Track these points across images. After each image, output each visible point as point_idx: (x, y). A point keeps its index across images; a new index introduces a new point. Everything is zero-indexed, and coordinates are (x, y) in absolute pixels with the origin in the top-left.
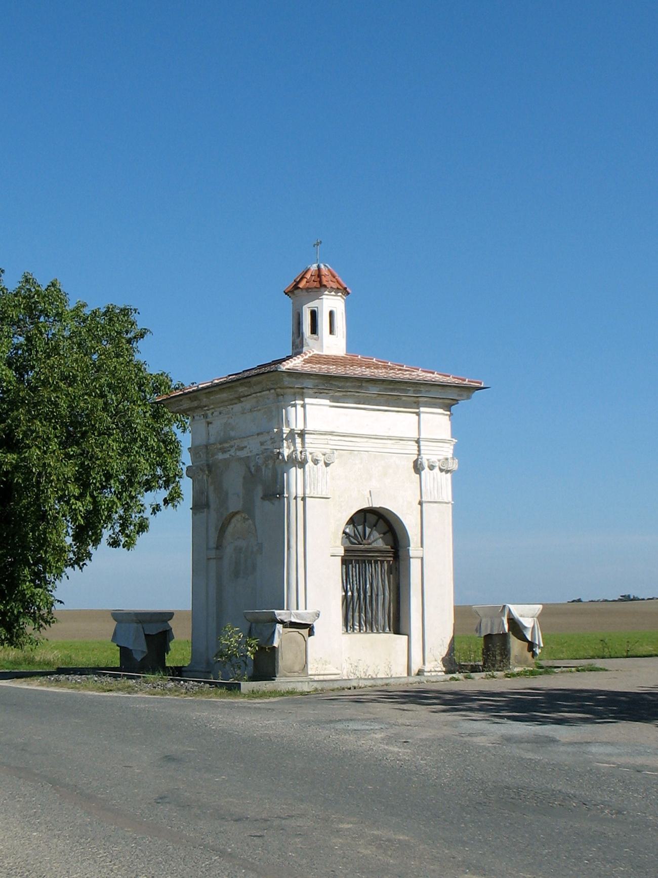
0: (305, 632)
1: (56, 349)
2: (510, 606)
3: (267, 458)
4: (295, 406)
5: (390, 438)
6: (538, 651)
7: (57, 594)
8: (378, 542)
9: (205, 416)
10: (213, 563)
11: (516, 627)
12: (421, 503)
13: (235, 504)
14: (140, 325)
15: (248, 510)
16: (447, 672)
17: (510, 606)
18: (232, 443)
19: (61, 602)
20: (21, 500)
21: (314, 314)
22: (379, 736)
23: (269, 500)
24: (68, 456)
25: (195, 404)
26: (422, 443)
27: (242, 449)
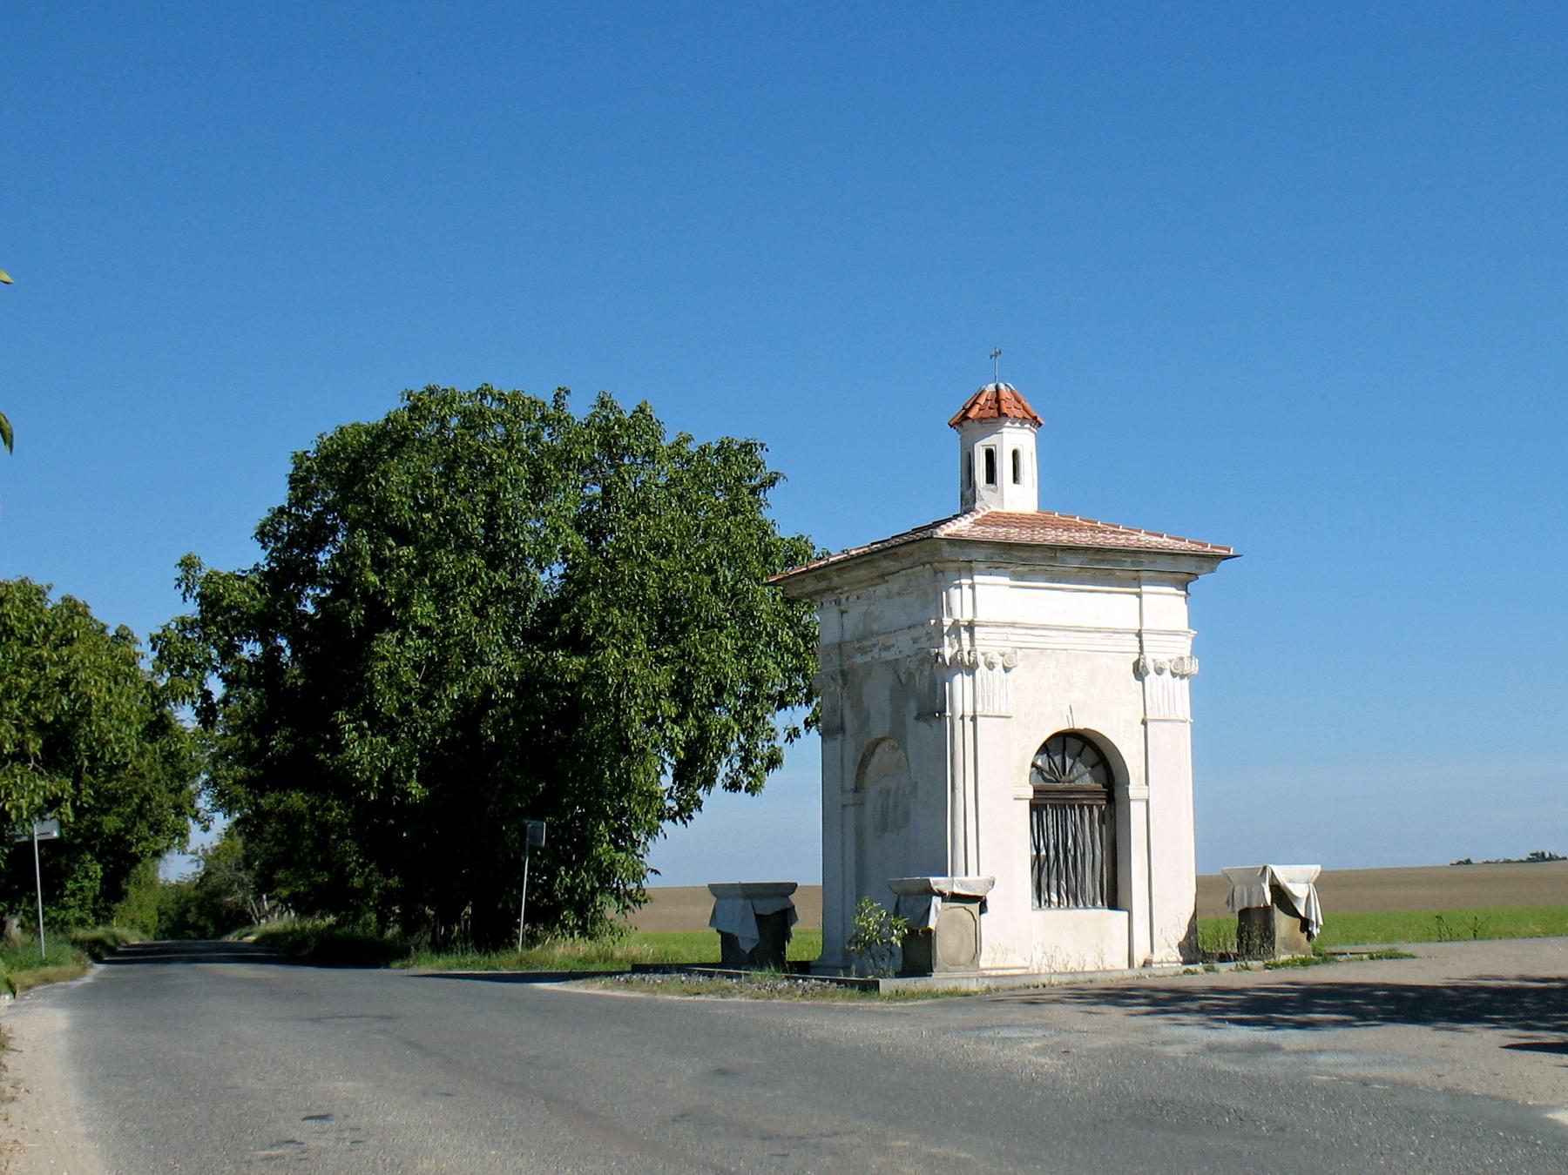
0: (975, 907)
1: (644, 504)
3: (922, 661)
4: (960, 586)
5: (1098, 630)
6: (1316, 931)
7: (650, 861)
8: (1084, 778)
9: (838, 602)
10: (850, 811)
11: (1282, 897)
12: (1144, 722)
13: (879, 728)
14: (770, 468)
15: (898, 735)
16: (1184, 963)
18: (874, 640)
19: (657, 872)
20: (592, 724)
21: (990, 455)
22: (1031, 1046)
23: (926, 721)
24: (661, 660)
25: (823, 585)
27: (887, 648)
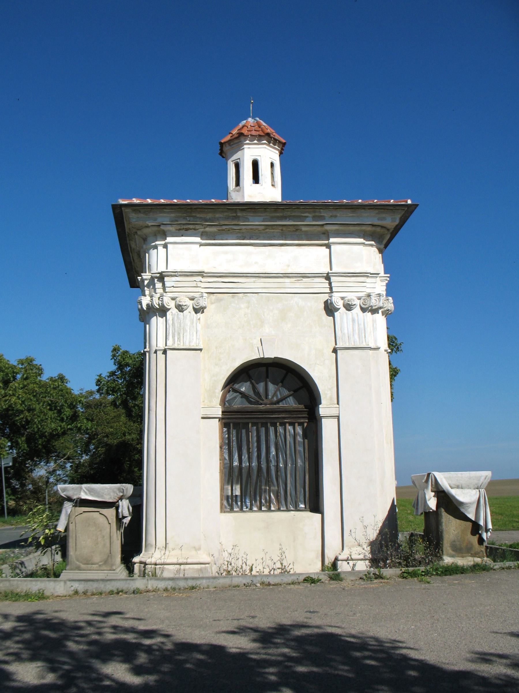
2: (433, 473)
4: (156, 247)
5: (286, 276)
11: (445, 500)
12: (335, 351)
17: (433, 473)
26: (333, 279)
